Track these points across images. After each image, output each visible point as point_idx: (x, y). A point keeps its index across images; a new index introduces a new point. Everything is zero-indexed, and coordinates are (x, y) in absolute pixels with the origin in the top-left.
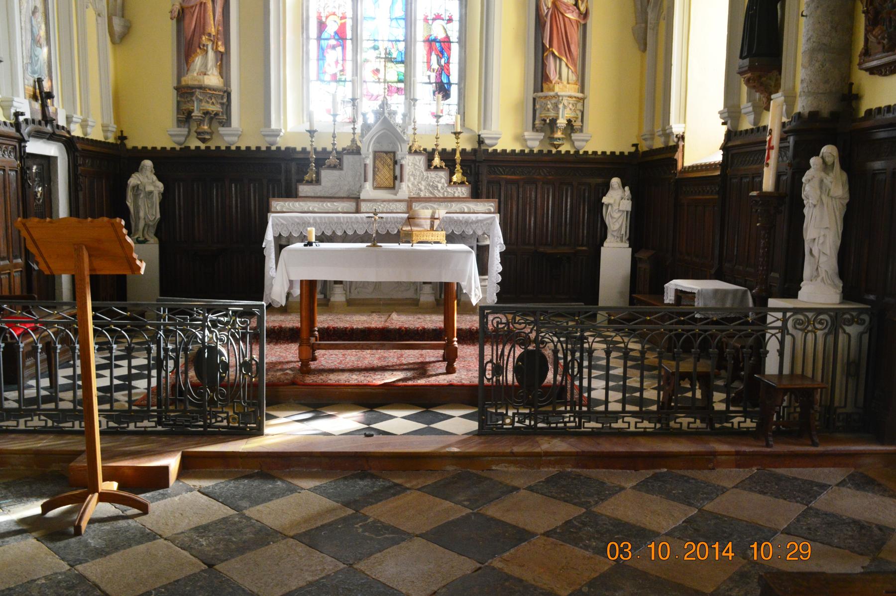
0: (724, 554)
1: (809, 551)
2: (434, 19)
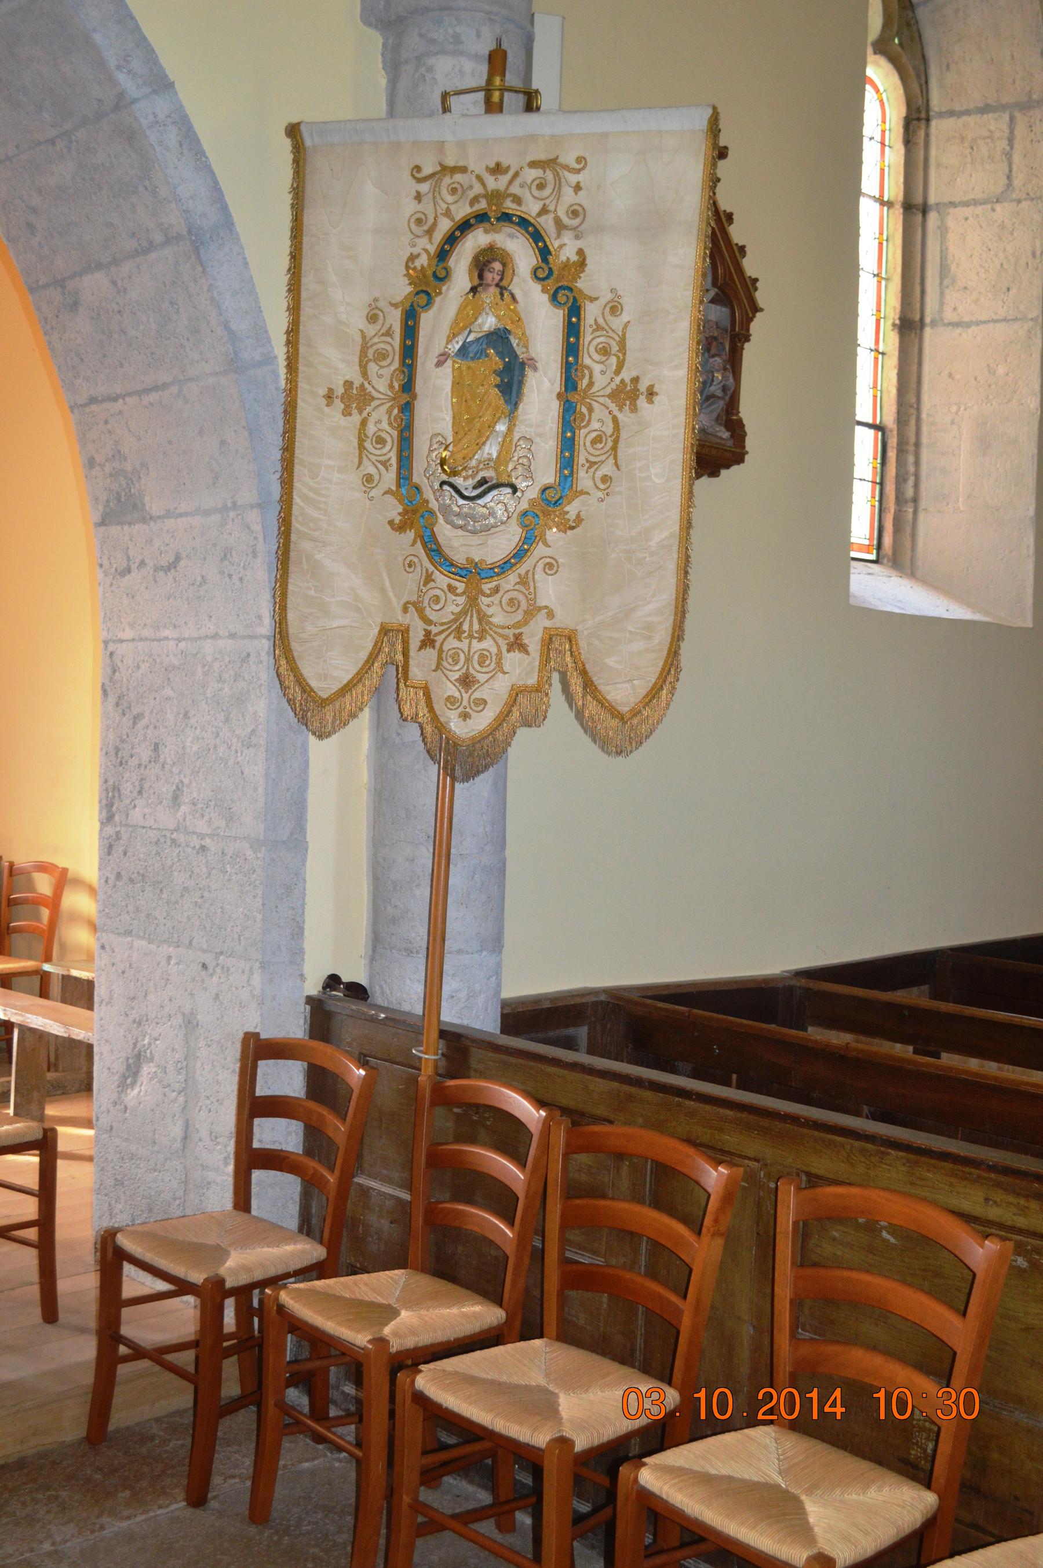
0: (827, 1409)
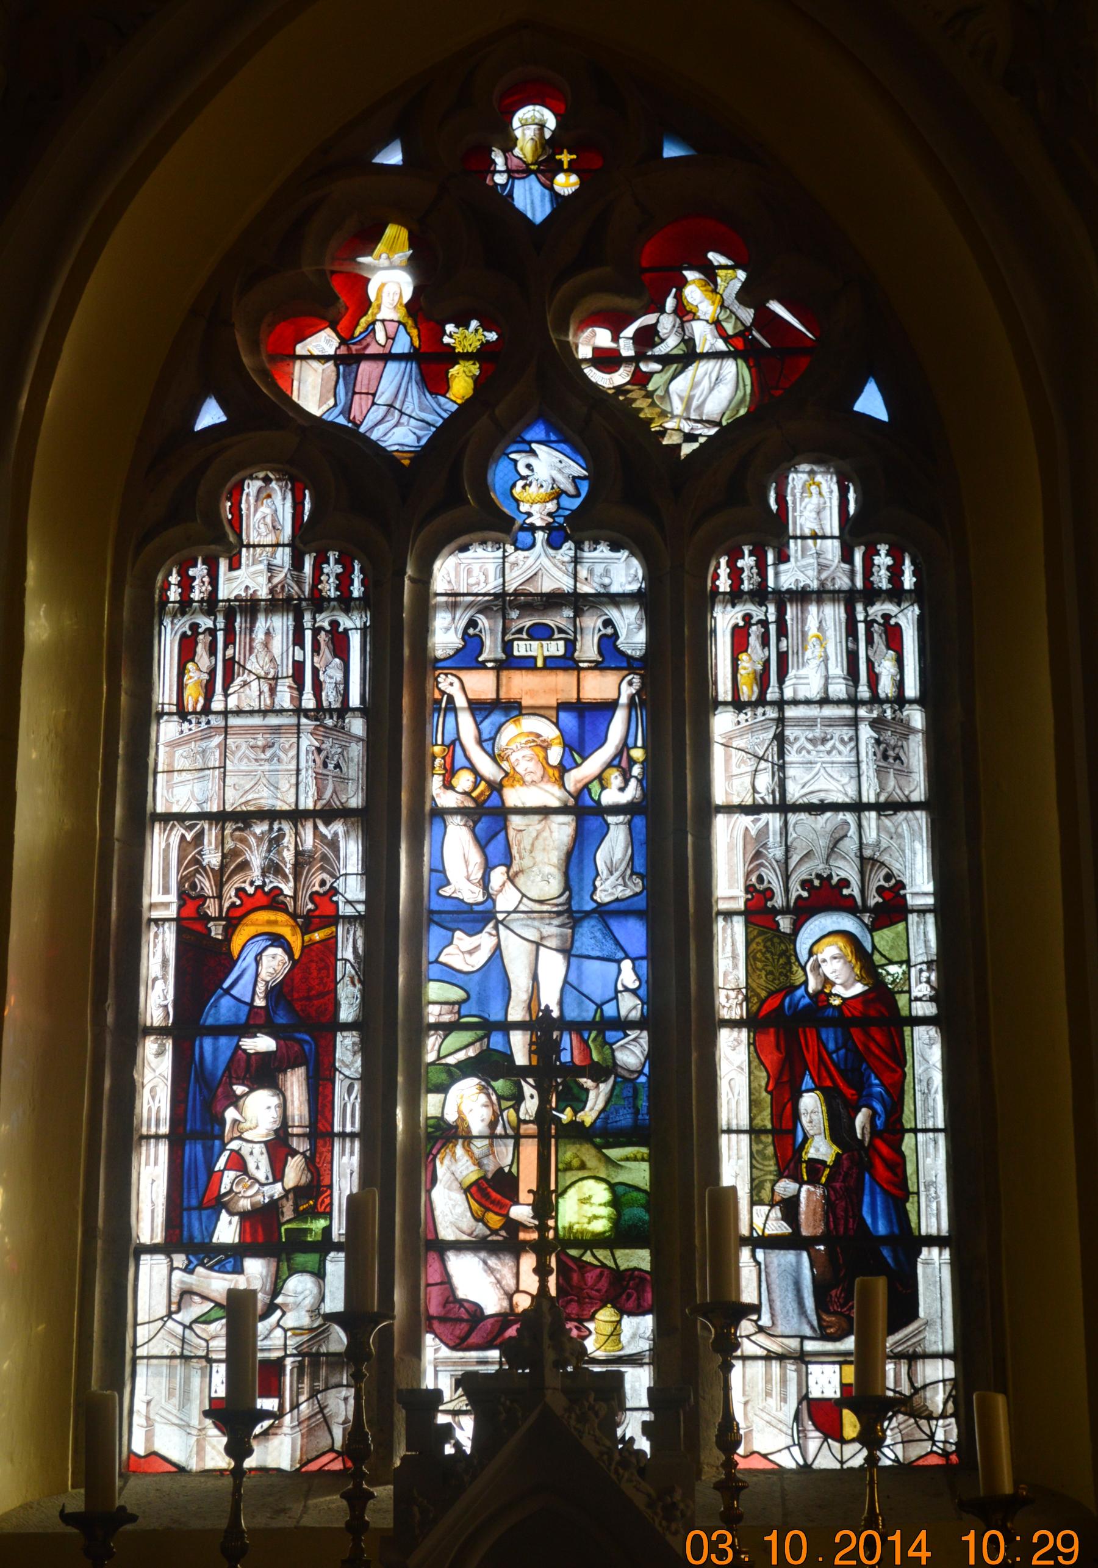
0: (911, 1553)
1: (1076, 1547)
2: (802, 912)
